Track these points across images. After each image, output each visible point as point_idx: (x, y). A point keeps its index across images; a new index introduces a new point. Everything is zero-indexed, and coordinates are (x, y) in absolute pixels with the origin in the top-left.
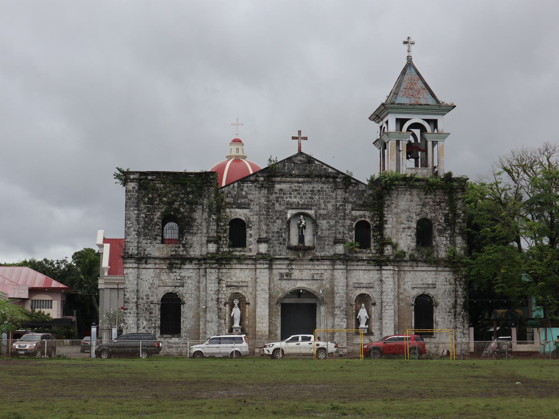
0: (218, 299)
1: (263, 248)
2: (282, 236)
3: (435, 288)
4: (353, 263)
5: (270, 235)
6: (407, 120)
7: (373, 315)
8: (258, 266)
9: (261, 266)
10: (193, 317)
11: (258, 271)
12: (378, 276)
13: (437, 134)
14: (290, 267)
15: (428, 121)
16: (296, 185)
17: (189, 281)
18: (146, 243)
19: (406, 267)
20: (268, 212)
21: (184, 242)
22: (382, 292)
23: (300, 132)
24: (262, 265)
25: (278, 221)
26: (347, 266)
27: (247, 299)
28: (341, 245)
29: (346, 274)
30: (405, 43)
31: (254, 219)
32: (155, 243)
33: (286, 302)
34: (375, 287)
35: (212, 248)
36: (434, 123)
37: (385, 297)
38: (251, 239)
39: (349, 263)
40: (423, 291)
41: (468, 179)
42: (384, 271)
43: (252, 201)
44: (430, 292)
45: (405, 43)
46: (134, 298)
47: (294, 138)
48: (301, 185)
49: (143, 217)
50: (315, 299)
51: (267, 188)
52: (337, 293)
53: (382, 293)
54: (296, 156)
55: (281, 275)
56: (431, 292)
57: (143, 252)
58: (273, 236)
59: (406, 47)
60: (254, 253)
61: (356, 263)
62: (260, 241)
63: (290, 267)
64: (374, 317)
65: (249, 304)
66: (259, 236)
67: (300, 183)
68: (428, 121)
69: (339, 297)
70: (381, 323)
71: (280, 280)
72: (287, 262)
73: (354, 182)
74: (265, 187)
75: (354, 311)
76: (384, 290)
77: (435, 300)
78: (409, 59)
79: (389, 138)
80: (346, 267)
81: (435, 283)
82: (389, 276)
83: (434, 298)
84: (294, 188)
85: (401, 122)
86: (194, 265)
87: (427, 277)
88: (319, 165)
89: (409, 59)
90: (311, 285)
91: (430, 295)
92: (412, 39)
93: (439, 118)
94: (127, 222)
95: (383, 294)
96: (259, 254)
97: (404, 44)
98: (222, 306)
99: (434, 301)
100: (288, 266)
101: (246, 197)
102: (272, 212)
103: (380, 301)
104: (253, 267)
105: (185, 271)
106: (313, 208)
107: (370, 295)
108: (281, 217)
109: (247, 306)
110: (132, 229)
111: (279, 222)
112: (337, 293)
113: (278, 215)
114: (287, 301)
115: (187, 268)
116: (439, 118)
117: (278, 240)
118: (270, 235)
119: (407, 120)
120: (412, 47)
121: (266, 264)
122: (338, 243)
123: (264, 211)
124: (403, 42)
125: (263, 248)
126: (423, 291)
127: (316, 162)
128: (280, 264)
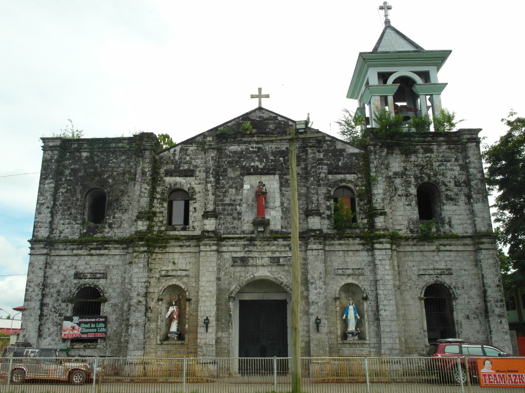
0: (146, 293)
1: (210, 224)
2: (236, 209)
3: (451, 274)
4: (333, 242)
5: (220, 208)
6: (391, 73)
7: (365, 313)
8: (202, 248)
9: (208, 248)
10: (299, 332)
11: (202, 254)
12: (370, 258)
13: (426, 95)
14: (246, 249)
15: (420, 74)
16: (254, 146)
17: (115, 271)
18: (63, 224)
19: (408, 247)
20: (219, 179)
21: (110, 221)
22: (376, 281)
23: (260, 90)
24: (208, 247)
25: (230, 190)
26: (325, 245)
27: (187, 294)
28: (316, 217)
29: (323, 257)
30: (381, 8)
31: (198, 188)
32: (74, 223)
33: (246, 299)
34: (365, 274)
35: (142, 226)
36: (425, 76)
37: (382, 287)
38: (196, 214)
39: (327, 242)
40: (435, 279)
41: (480, 130)
42: (377, 250)
43: (196, 167)
44: (446, 280)
45: (381, 8)
46: (39, 295)
47: (253, 97)
48: (260, 145)
49: (62, 192)
50: (285, 294)
51: (216, 149)
52: (312, 283)
53: (376, 283)
54: (254, 111)
55: (234, 260)
56: (446, 280)
57: (58, 235)
58: (224, 210)
59: (382, 12)
60: (198, 232)
61: (338, 242)
62: (206, 215)
63: (246, 249)
64: (368, 317)
65: (189, 300)
66: (205, 209)
67: (260, 144)
68: (420, 74)
69: (316, 289)
70: (378, 326)
71: (233, 266)
72: (242, 242)
73: (330, 139)
74: (213, 149)
75: (338, 308)
76: (378, 278)
77: (453, 291)
78: (387, 22)
79: (371, 94)
80: (324, 247)
81: (450, 267)
82: (384, 257)
83: (452, 289)
84: (251, 149)
85: (383, 77)
86: (122, 251)
87: (438, 259)
88: (283, 121)
89: (387, 22)
90: (275, 273)
91: (445, 285)
92: (389, 4)
93: (431, 69)
94: (40, 197)
95: (378, 283)
96: (203, 232)
97: (380, 9)
98: (152, 304)
99: (452, 292)
100: (244, 248)
101: (191, 163)
102: (224, 179)
103: (374, 293)
104: (196, 250)
105: (110, 258)
106: (277, 172)
107: (360, 286)
108: (234, 185)
109: (188, 303)
110: (45, 206)
111: (232, 192)
112: (312, 283)
113: (231, 183)
114: (247, 297)
115: (112, 254)
116: (431, 69)
117: (231, 215)
118: (220, 208)
119: (391, 73)
120: (390, 12)
121: (213, 244)
122: (311, 216)
123: (213, 177)
124: (378, 7)
125: (210, 224)
126: (435, 279)
127: (279, 118)
128: (232, 246)
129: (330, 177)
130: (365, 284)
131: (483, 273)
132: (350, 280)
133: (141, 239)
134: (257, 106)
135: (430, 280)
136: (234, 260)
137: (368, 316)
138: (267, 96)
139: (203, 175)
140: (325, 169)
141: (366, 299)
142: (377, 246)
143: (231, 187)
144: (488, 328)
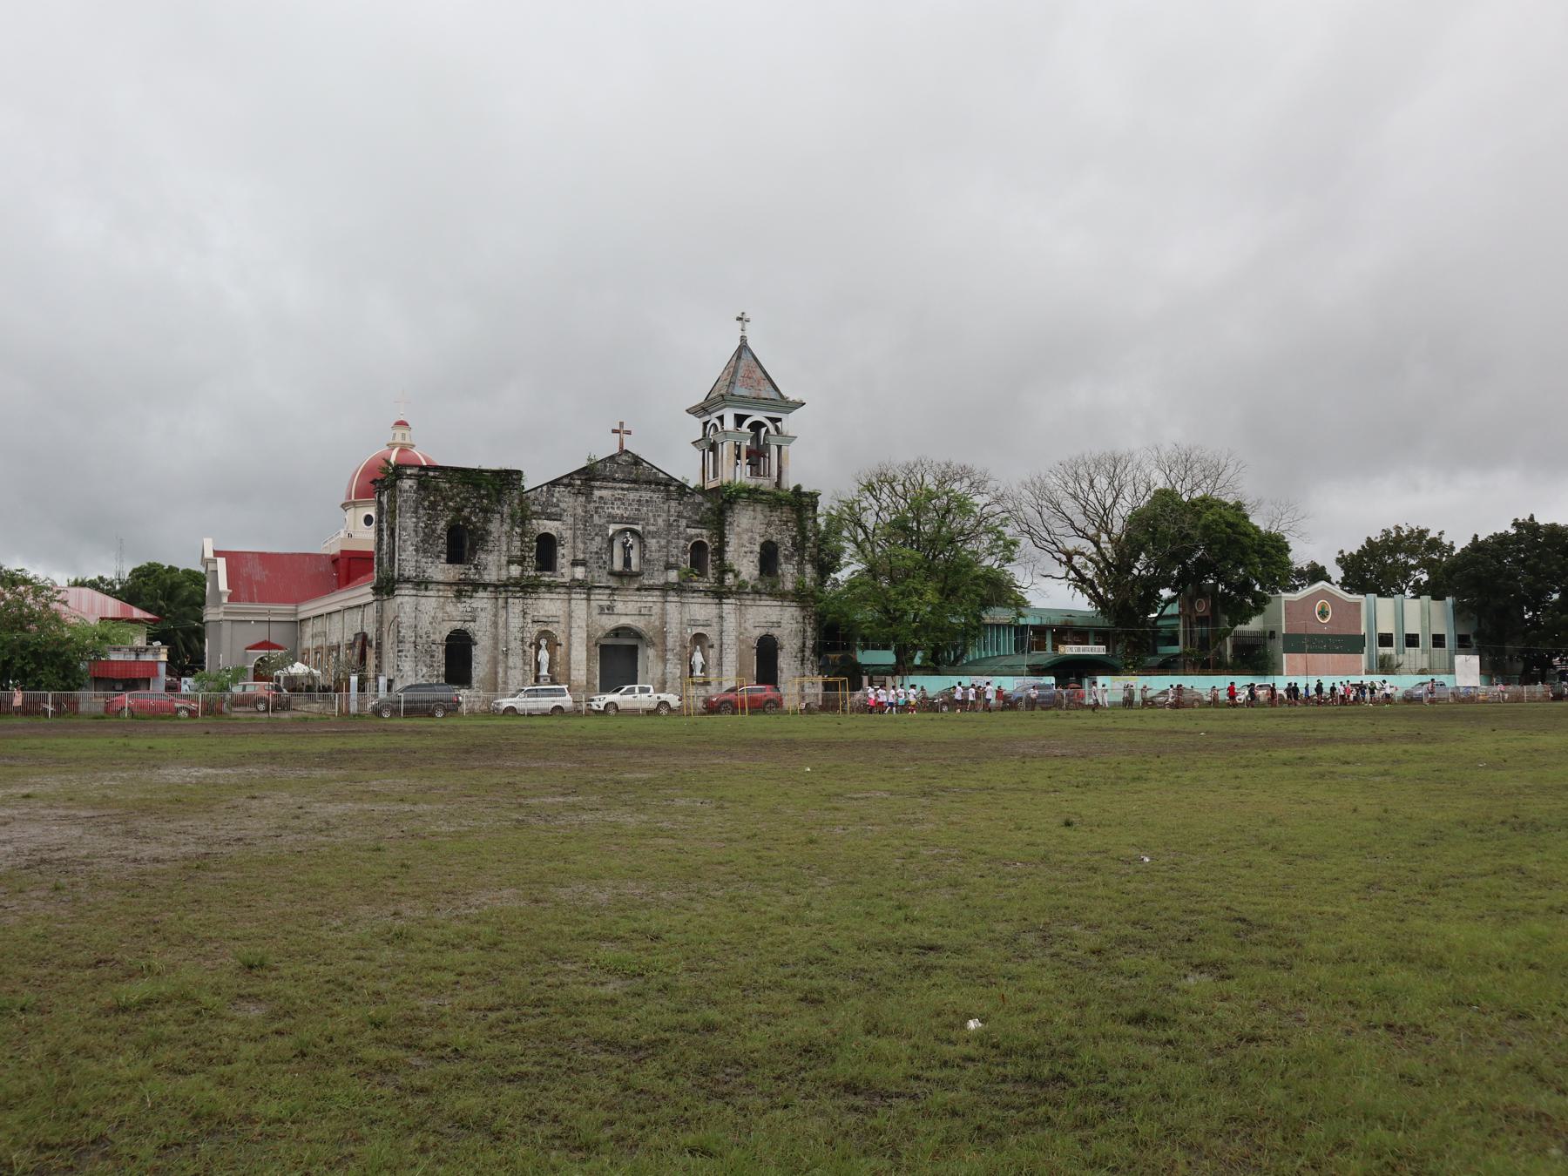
1: (579, 573)
17: (483, 614)
23: (621, 424)
30: (739, 319)
31: (568, 534)
55: (602, 608)
56: (775, 632)
59: (739, 324)
60: (567, 579)
62: (575, 563)
65: (560, 645)
78: (743, 339)
85: (740, 419)
89: (743, 339)
96: (573, 580)
101: (558, 506)
104: (566, 597)
125: (579, 573)
129: (688, 530)
130: (712, 634)
131: (483, 1007)
132: (700, 630)
133: (515, 585)
134: (616, 450)
135: (763, 632)
136: (602, 608)
137: (713, 661)
138: (629, 433)
139: (570, 521)
140: (683, 523)
141: (712, 646)
142: (725, 601)
143: (596, 535)
144: (1287, 770)
